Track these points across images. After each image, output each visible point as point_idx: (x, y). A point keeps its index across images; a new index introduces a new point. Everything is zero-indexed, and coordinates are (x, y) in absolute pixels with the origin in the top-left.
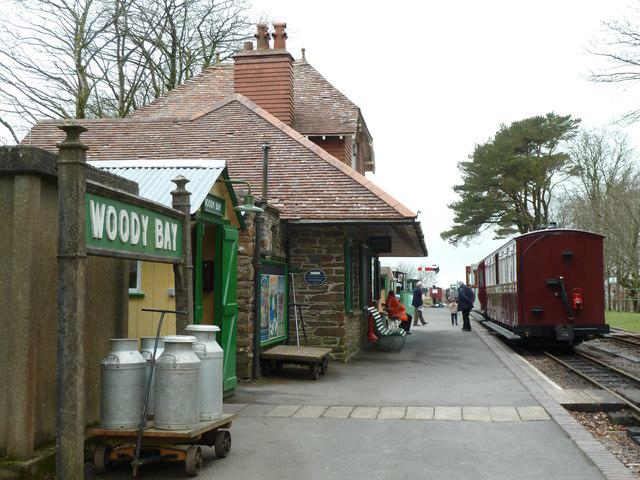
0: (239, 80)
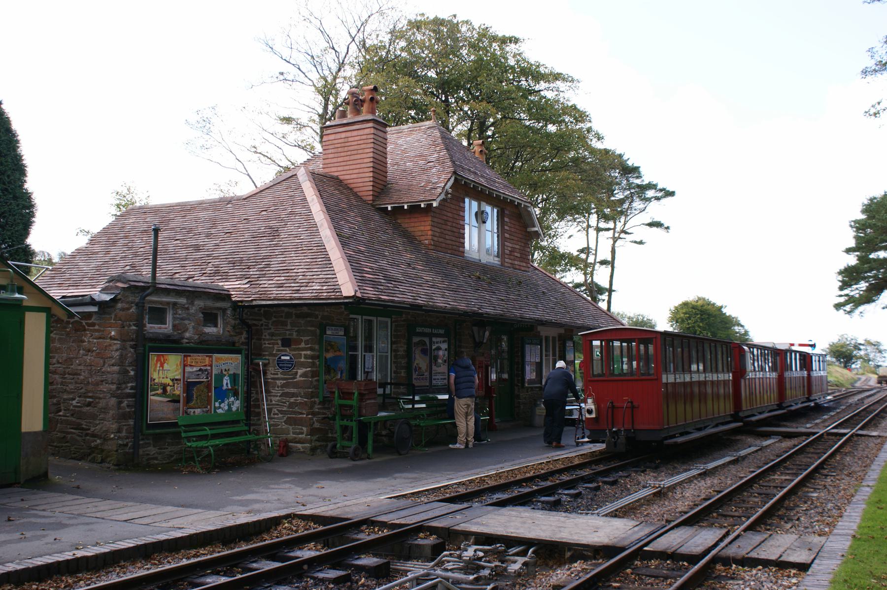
0: (327, 152)
